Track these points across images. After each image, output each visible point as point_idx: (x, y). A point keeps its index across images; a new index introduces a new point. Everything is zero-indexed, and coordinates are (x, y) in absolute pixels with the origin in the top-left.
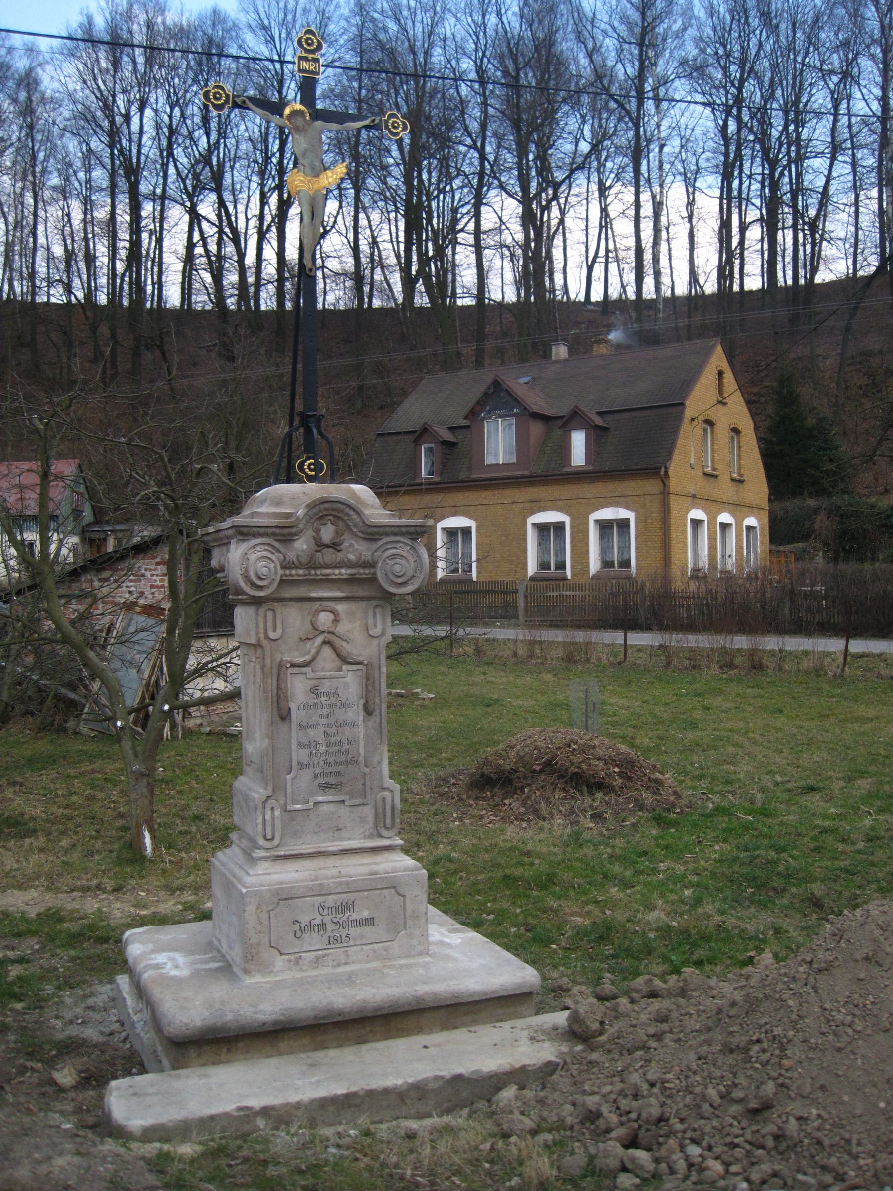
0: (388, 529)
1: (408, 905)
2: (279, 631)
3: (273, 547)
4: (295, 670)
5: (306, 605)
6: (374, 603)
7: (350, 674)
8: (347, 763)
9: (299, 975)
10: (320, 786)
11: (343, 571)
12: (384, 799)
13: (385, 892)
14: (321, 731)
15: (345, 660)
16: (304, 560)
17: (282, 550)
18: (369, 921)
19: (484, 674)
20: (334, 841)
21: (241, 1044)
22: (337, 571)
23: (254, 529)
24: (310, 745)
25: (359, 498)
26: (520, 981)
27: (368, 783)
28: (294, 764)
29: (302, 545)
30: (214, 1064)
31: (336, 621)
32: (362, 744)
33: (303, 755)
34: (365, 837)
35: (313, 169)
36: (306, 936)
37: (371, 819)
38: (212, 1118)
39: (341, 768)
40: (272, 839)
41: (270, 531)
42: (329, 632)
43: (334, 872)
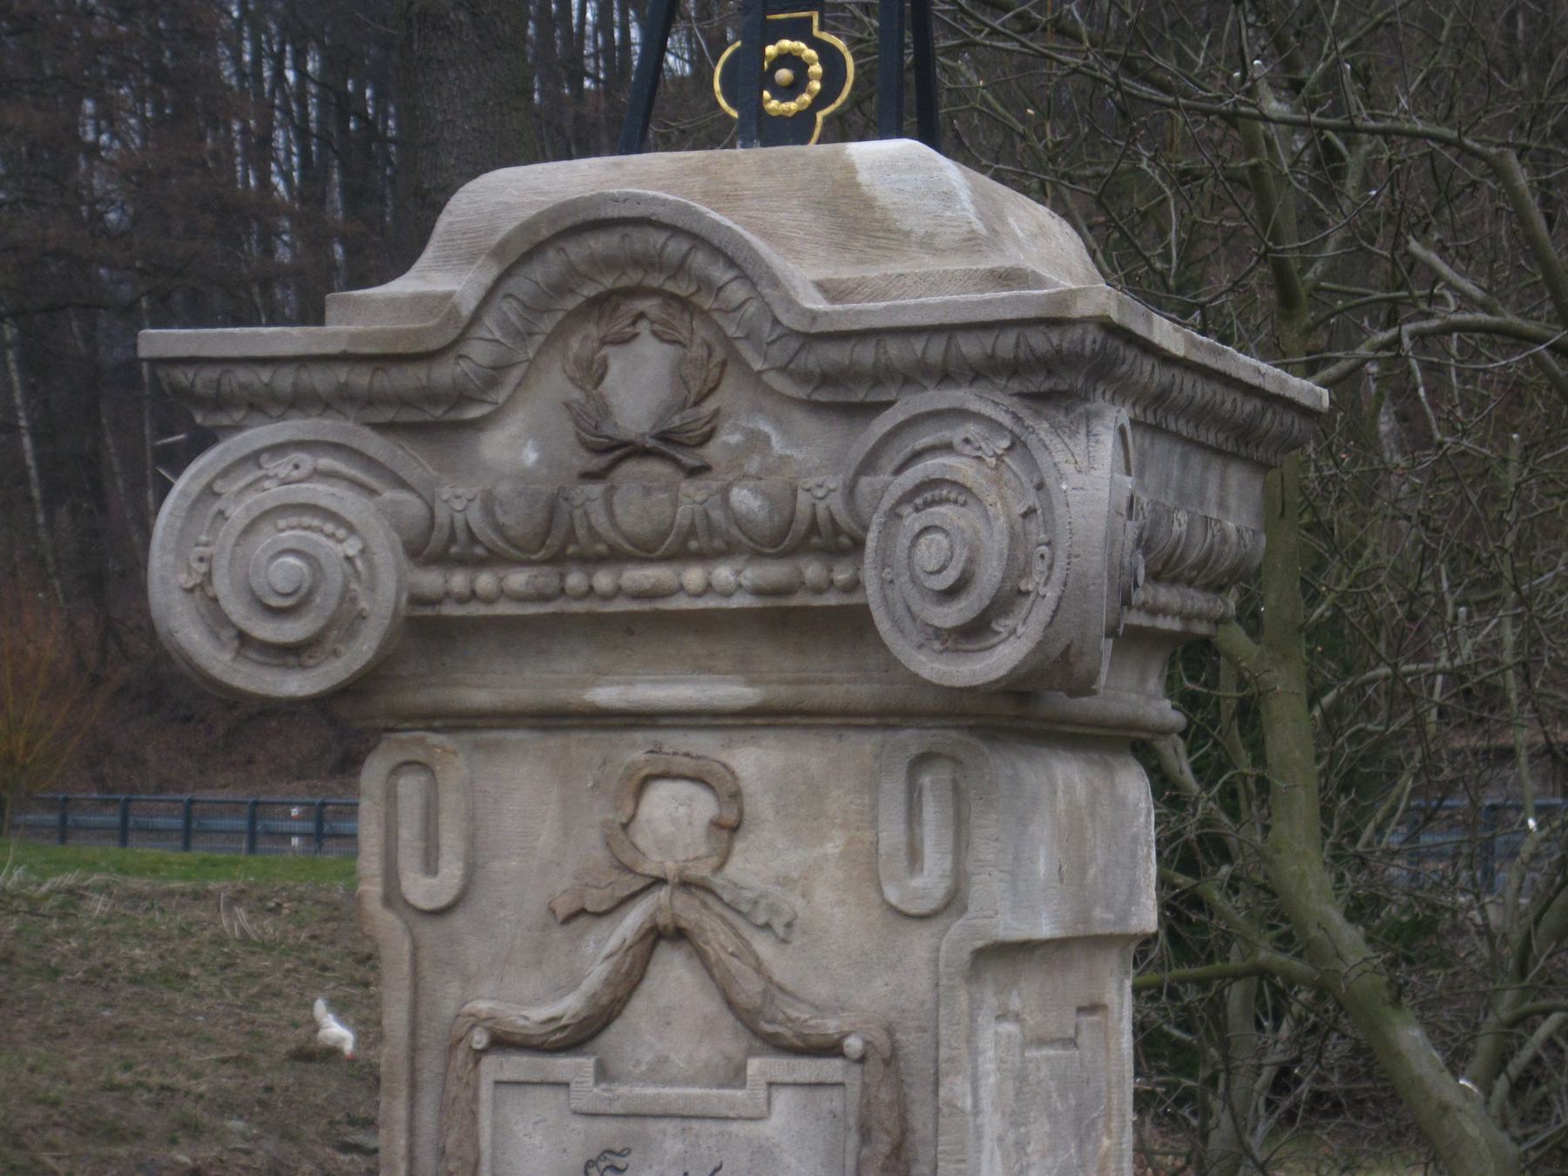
0: (894, 350)
2: (451, 871)
3: (369, 462)
4: (517, 1065)
5: (584, 747)
6: (911, 740)
7: (782, 1099)
11: (723, 573)
15: (766, 1030)
16: (518, 520)
17: (411, 473)
19: (245, 1077)
22: (694, 576)
23: (243, 375)
25: (868, 203)
29: (517, 448)
31: (728, 829)
42: (686, 884)
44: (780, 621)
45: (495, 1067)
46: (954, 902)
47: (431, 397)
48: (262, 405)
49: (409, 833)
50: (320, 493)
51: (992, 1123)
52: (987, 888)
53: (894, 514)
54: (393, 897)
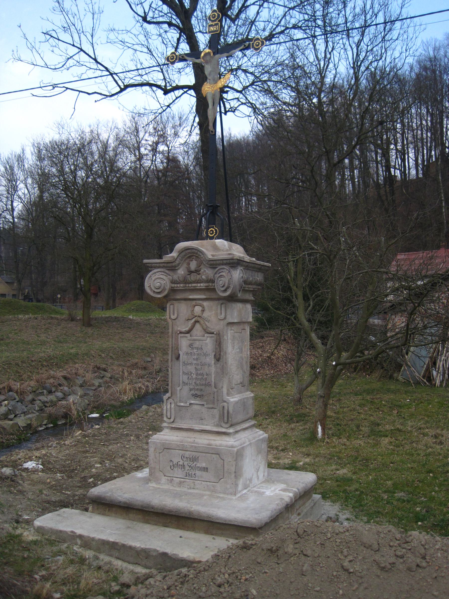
0: (218, 262)
1: (225, 466)
2: (176, 315)
3: (167, 273)
4: (182, 335)
5: (189, 302)
6: (221, 302)
7: (208, 338)
8: (205, 385)
9: (172, 488)
10: (193, 395)
11: (202, 285)
12: (223, 407)
13: (213, 455)
14: (194, 367)
16: (181, 279)
18: (205, 469)
20: (199, 424)
21: (114, 509)
22: (199, 285)
24: (189, 374)
25: (217, 246)
26: (246, 519)
27: (216, 397)
28: (181, 382)
29: (181, 272)
30: (103, 514)
31: (203, 311)
32: (213, 376)
33: (185, 378)
34: (214, 426)
35: (214, 80)
36: (176, 469)
37: (217, 416)
38: (61, 531)
39: (203, 387)
40: (170, 418)
41: (161, 265)
42: (199, 316)
43: (191, 440)
44: (208, 289)
45: (180, 335)
46: (225, 318)
47: (172, 267)
48: (156, 267)
49: (172, 311)
50: (161, 276)
51: (230, 341)
52: (228, 317)
53: (218, 279)
54: (170, 318)
